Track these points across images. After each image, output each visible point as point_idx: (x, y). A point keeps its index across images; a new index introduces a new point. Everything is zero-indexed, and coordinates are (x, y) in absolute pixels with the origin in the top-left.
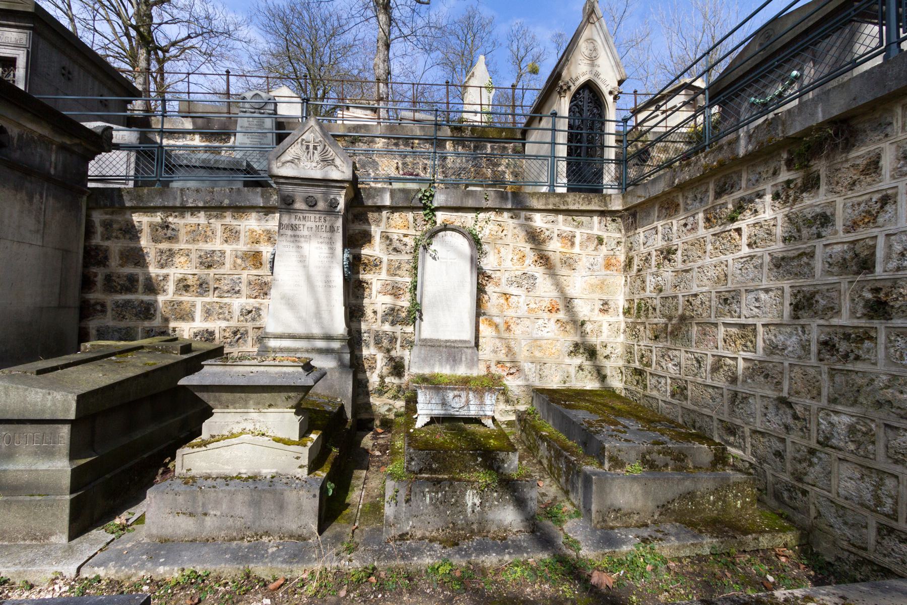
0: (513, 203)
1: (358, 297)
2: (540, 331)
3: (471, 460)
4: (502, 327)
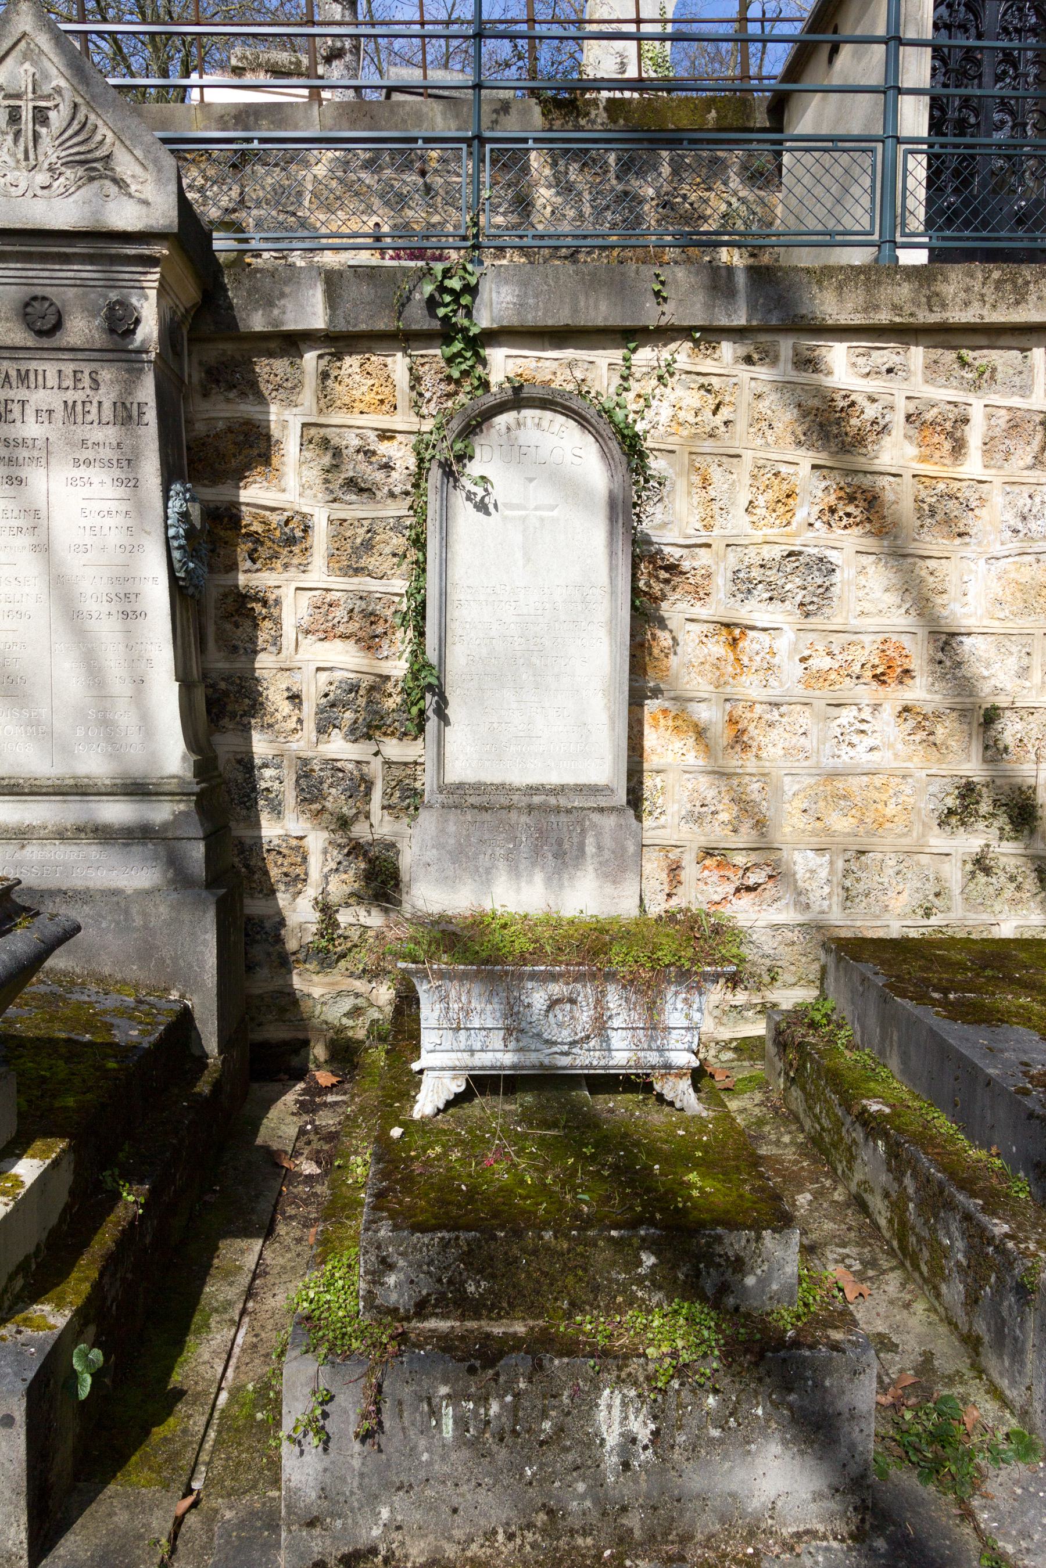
0: (752, 308)
1: (235, 649)
2: (844, 746)
3: (614, 1263)
4: (721, 734)
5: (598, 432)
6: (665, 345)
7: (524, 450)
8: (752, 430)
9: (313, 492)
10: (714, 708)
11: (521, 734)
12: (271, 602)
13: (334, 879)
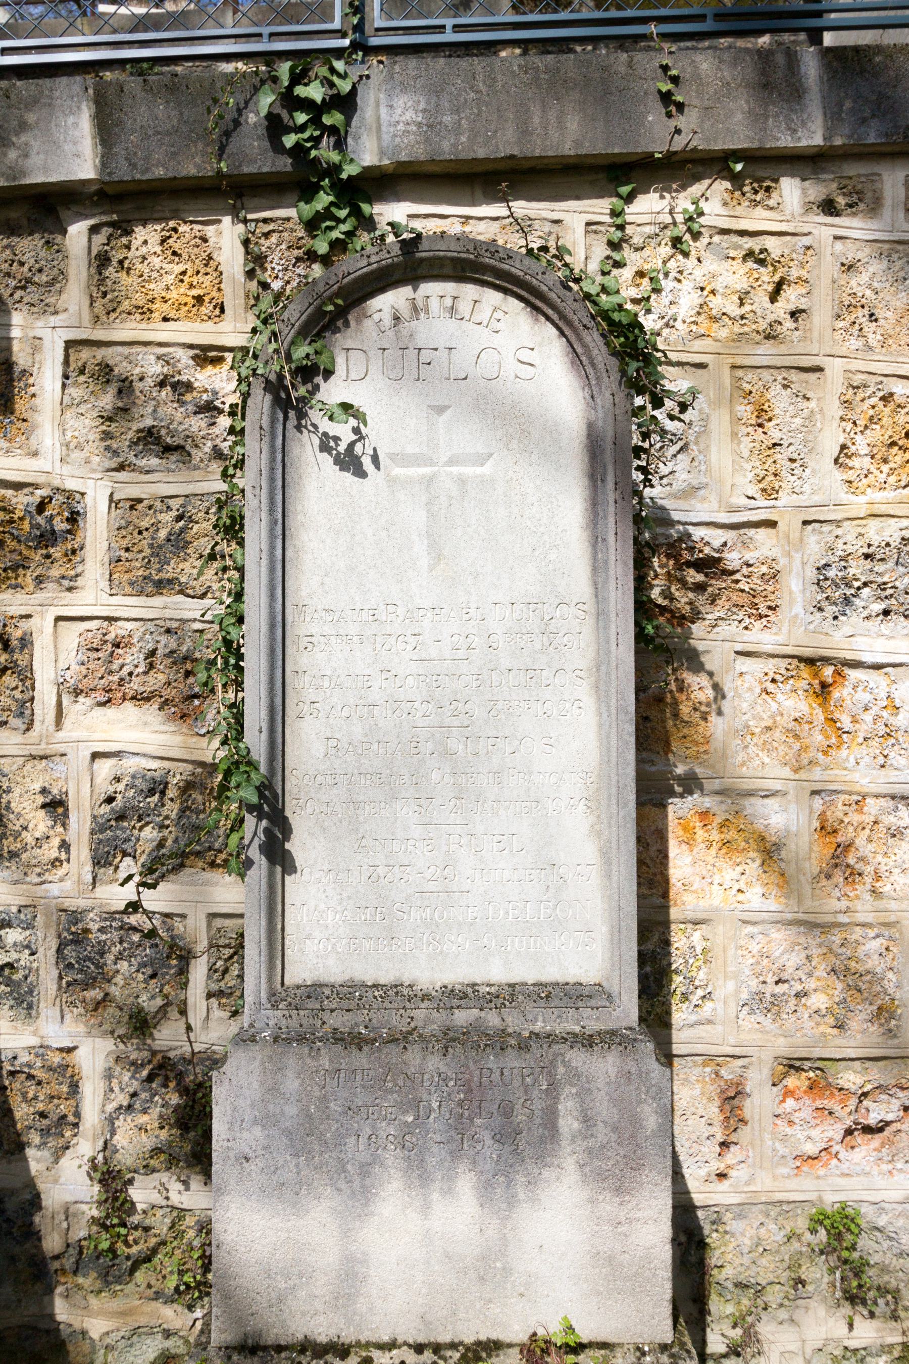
0: (833, 116)
5: (562, 316)
6: (684, 187)
7: (426, 356)
8: (841, 324)
9: (85, 454)
10: (793, 807)
11: (431, 886)
12: (15, 643)
13: (124, 1124)
